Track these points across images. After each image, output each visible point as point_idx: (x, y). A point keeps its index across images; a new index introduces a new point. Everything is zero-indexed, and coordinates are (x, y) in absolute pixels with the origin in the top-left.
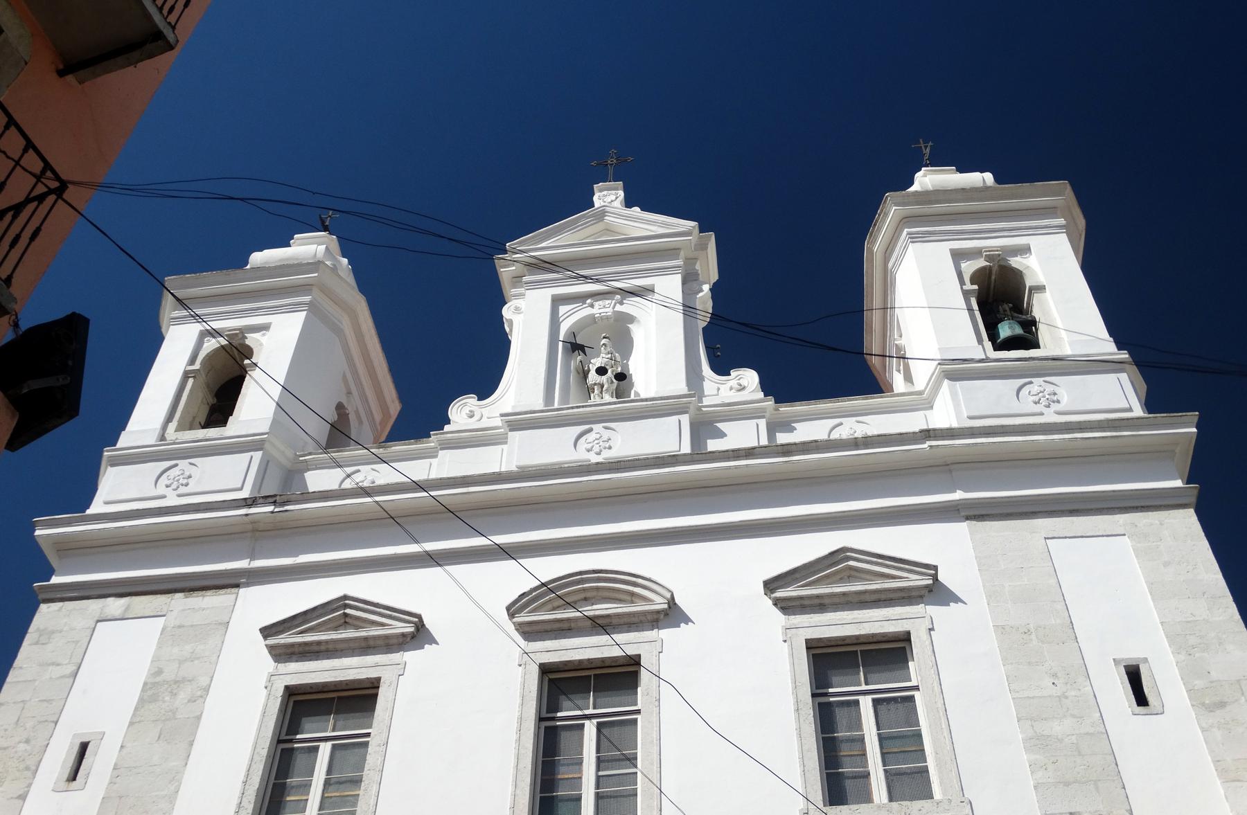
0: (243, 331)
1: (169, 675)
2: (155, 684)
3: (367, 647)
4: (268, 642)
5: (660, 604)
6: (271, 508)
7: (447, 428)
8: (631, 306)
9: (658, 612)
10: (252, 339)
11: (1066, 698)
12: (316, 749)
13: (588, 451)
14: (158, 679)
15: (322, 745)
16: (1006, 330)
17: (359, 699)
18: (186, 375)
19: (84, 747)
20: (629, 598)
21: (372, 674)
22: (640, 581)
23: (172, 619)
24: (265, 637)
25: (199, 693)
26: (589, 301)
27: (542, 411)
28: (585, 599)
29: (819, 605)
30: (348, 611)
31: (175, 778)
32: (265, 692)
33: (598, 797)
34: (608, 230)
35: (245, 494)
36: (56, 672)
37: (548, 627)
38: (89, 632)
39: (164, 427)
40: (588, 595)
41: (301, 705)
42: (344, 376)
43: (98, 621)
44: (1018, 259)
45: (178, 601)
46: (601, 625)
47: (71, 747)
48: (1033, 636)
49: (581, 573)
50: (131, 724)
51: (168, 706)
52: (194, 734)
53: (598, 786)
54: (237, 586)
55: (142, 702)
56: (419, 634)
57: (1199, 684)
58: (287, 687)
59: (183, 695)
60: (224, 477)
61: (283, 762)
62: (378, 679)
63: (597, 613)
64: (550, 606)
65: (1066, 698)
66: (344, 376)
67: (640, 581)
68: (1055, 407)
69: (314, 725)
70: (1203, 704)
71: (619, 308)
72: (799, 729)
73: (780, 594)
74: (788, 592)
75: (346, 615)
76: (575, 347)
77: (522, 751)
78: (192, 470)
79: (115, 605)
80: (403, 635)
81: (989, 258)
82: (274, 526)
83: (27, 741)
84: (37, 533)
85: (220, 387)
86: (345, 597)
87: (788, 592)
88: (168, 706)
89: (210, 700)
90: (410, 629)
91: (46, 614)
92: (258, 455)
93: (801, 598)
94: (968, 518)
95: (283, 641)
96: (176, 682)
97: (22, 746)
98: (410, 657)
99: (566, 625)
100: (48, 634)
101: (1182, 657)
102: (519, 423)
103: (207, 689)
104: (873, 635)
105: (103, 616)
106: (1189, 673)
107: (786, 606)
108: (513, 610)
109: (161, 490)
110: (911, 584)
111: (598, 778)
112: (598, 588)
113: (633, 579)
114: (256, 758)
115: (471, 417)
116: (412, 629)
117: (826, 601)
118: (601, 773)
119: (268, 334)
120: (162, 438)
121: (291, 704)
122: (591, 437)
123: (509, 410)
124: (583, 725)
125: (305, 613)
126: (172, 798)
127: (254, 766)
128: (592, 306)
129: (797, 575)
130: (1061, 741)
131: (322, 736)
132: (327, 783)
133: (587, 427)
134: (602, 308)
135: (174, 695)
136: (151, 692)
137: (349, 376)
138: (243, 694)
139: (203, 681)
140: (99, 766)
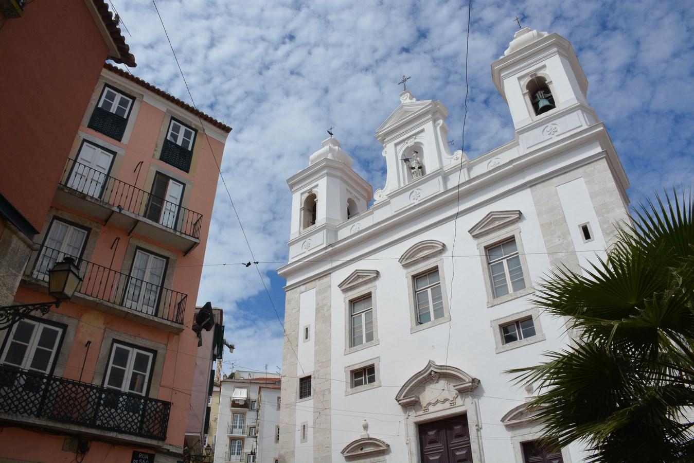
0: (311, 189)
2: (318, 308)
3: (366, 283)
4: (342, 289)
5: (440, 248)
6: (331, 248)
7: (375, 203)
8: (418, 139)
9: (441, 250)
10: (314, 191)
12: (361, 315)
14: (319, 306)
16: (543, 103)
17: (368, 297)
19: (307, 329)
21: (435, 265)
26: (406, 141)
29: (487, 233)
30: (359, 274)
31: (329, 332)
33: (434, 311)
34: (406, 112)
35: (324, 246)
36: (294, 311)
39: (300, 230)
40: (420, 250)
41: (353, 303)
42: (347, 190)
44: (542, 72)
45: (318, 283)
46: (426, 258)
50: (316, 320)
51: (323, 313)
52: (331, 320)
53: (434, 308)
54: (330, 273)
55: (317, 314)
56: (520, 216)
57: (605, 226)
58: (349, 301)
59: (325, 309)
60: (318, 242)
62: (371, 292)
66: (347, 190)
68: (556, 134)
70: (607, 234)
71: (416, 141)
73: (474, 234)
74: (477, 232)
75: (358, 275)
76: (406, 160)
78: (310, 242)
79: (303, 288)
80: (374, 277)
81: (531, 76)
82: (333, 252)
83: (294, 331)
84: (278, 273)
86: (356, 270)
87: (477, 232)
88: (323, 313)
89: (332, 309)
90: (375, 275)
91: (289, 295)
92: (325, 231)
94: (530, 187)
96: (323, 306)
97: (293, 333)
98: (520, 225)
101: (600, 218)
102: (392, 196)
103: (330, 306)
104: (504, 239)
106: (601, 223)
107: (476, 237)
108: (401, 261)
109: (304, 250)
110: (512, 218)
111: (433, 305)
112: (423, 247)
115: (380, 197)
117: (488, 232)
119: (319, 187)
120: (300, 233)
121: (415, 280)
123: (389, 193)
124: (502, 262)
126: (330, 338)
128: (407, 143)
132: (366, 324)
133: (412, 191)
134: (411, 143)
135: (323, 310)
136: (319, 309)
137: (349, 189)
138: (339, 303)
139: (329, 304)
140: (312, 333)
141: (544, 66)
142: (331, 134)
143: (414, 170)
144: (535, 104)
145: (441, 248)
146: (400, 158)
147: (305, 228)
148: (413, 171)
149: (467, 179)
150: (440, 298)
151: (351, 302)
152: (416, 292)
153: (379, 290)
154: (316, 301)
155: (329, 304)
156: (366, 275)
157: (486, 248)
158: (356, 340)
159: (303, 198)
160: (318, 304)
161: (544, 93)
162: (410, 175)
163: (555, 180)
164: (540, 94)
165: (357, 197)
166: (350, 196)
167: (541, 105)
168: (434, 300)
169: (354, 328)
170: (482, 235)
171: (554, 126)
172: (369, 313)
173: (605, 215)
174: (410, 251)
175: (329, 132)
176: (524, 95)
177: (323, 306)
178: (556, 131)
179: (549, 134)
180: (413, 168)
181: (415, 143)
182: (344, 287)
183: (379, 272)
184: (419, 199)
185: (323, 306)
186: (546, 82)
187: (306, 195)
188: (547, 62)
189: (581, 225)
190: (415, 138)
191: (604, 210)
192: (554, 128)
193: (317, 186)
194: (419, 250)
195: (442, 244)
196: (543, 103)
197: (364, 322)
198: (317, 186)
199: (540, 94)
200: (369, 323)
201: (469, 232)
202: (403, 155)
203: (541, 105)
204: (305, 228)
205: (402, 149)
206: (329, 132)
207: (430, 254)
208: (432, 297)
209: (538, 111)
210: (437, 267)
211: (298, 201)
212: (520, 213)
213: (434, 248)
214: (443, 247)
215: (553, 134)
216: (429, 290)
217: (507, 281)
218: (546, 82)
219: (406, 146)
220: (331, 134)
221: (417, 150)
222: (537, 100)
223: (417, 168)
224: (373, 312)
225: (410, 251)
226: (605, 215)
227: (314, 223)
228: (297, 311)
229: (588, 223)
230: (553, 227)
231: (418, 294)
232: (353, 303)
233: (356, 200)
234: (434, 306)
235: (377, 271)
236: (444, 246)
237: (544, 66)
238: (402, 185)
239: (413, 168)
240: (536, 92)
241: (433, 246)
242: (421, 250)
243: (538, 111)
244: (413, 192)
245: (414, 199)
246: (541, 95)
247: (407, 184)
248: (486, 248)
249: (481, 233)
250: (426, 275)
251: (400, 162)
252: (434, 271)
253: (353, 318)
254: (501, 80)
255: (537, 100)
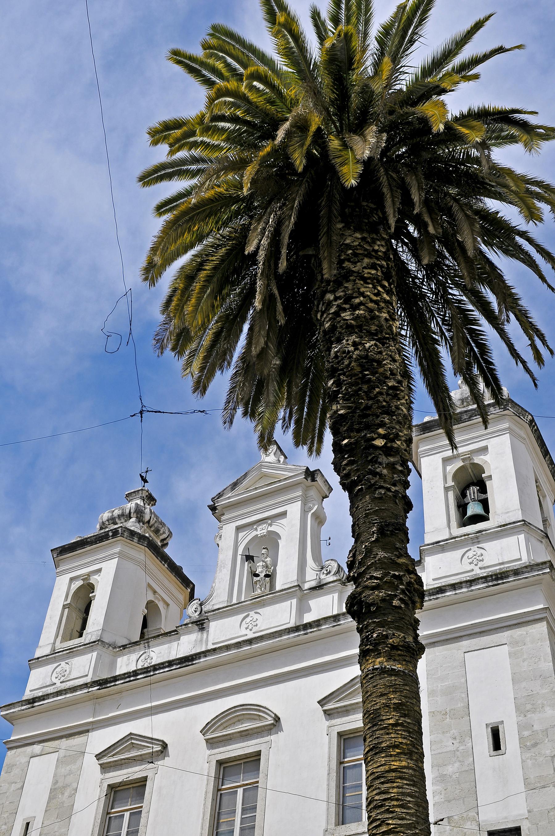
0: (89, 575)
1: (60, 784)
2: (55, 789)
4: (101, 762)
5: (270, 721)
11: (458, 751)
13: (470, 563)
14: (57, 786)
15: (126, 813)
16: (473, 509)
18: (64, 607)
19: (28, 824)
20: (257, 718)
22: (261, 708)
23: (62, 753)
24: (322, 706)
25: (73, 792)
27: (227, 607)
28: (239, 721)
30: (133, 741)
32: (99, 789)
34: (266, 475)
35: (88, 680)
36: (14, 787)
37: (220, 739)
38: (27, 763)
41: (115, 792)
43: (31, 757)
45: (64, 743)
46: (245, 735)
47: (22, 826)
48: (448, 716)
49: (235, 707)
50: (46, 811)
54: (88, 731)
57: (526, 733)
60: (83, 667)
61: (108, 823)
63: (241, 729)
64: (222, 727)
65: (458, 751)
67: (261, 708)
69: (352, 754)
70: (526, 746)
72: (328, 785)
75: (133, 743)
76: (249, 558)
77: (206, 810)
79: (37, 748)
81: (463, 460)
83: (6, 824)
85: (471, 484)
86: (131, 734)
90: (158, 748)
93: (110, 762)
95: (105, 761)
96: (63, 787)
99: (228, 737)
100: (12, 766)
103: (76, 790)
105: (33, 755)
106: (521, 727)
112: (243, 714)
113: (259, 708)
114: (96, 824)
116: (160, 748)
117: (348, 708)
118: (243, 817)
122: (248, 620)
125: (341, 688)
127: (95, 829)
128: (256, 529)
129: (334, 695)
130: (451, 777)
131: (237, 783)
134: (261, 530)
136: (55, 792)
138: (92, 786)
139: (74, 785)
141: (485, 450)
142: (145, 481)
143: (258, 578)
144: (462, 507)
145: (272, 722)
146: (240, 551)
147: (64, 640)
148: (255, 579)
149: (335, 613)
150: (254, 808)
151: (112, 788)
152: (219, 790)
153: (276, 752)
154: (55, 775)
155: (74, 785)
156: (144, 746)
157: (220, 763)
158: (348, 812)
159: (73, 586)
160: (55, 782)
161: (478, 490)
162: (252, 586)
163: (466, 644)
164: (473, 491)
165: (163, 600)
166: (151, 597)
167: (470, 512)
168: (244, 810)
169: (219, 813)
170: (338, 712)
171: (480, 551)
172: (252, 790)
173: (529, 716)
174: (223, 718)
175: (142, 477)
176: (447, 489)
177: (65, 787)
178: (482, 560)
179: (470, 563)
180: (257, 575)
181: (269, 532)
182: (105, 760)
183: (279, 719)
184: (255, 629)
185: (65, 787)
186: (483, 475)
187: (79, 583)
188: (493, 443)
189: (490, 724)
190: (270, 525)
191: (529, 707)
192: (479, 554)
193: (99, 570)
194: (248, 716)
195: (273, 716)
196: (473, 509)
197: (126, 830)
198: (99, 570)
199: (473, 491)
200: (132, 832)
201: (319, 702)
202: (247, 548)
203: (470, 512)
204: (64, 640)
205: (246, 537)
206: (142, 477)
207: (251, 729)
208: (243, 805)
209: (467, 520)
210: (258, 754)
211: (62, 589)
212: (165, 746)
213: (260, 720)
214: (274, 719)
215: (476, 565)
216: (240, 791)
217: (236, 826)
218: (483, 475)
219: (254, 533)
220: (145, 481)
221: (271, 542)
222: (466, 501)
223: (262, 575)
224: (143, 814)
225: (223, 718)
226: (529, 716)
227: (81, 635)
228: (19, 789)
229: (502, 722)
230: (448, 720)
231: (221, 794)
232: (115, 792)
233: (161, 605)
234: (243, 820)
235: (163, 742)
236: (277, 719)
237: (485, 450)
238: (235, 601)
239: (257, 575)
240: (467, 487)
241: (259, 716)
242: (240, 720)
243: (467, 520)
244: (60, 664)
245: (246, 628)
246: (474, 493)
247: (243, 600)
248: (220, 763)
249: (337, 708)
250: (130, 788)
251: (239, 557)
252: (253, 760)
253: (110, 818)
254: (419, 458)
255: (466, 501)
